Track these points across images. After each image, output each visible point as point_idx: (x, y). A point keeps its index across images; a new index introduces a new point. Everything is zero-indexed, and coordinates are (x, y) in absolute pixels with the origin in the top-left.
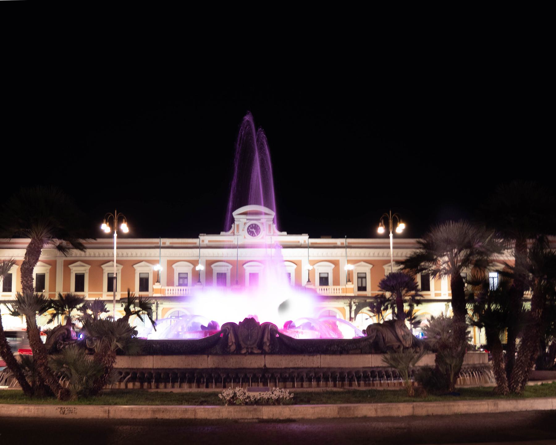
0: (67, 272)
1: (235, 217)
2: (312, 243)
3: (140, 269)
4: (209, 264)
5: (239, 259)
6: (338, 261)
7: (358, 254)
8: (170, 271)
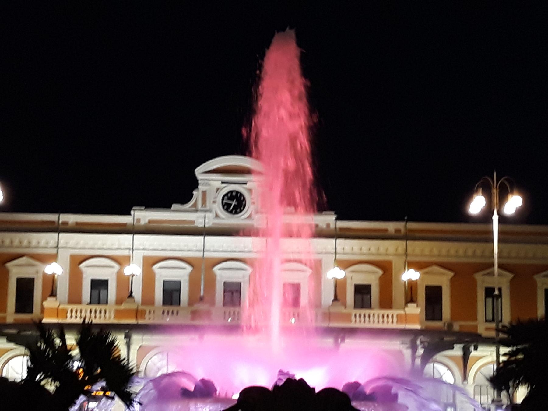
1: (199, 177)
3: (17, 271)
4: (77, 261)
5: (207, 255)
6: (390, 263)
7: (382, 250)
8: (75, 276)
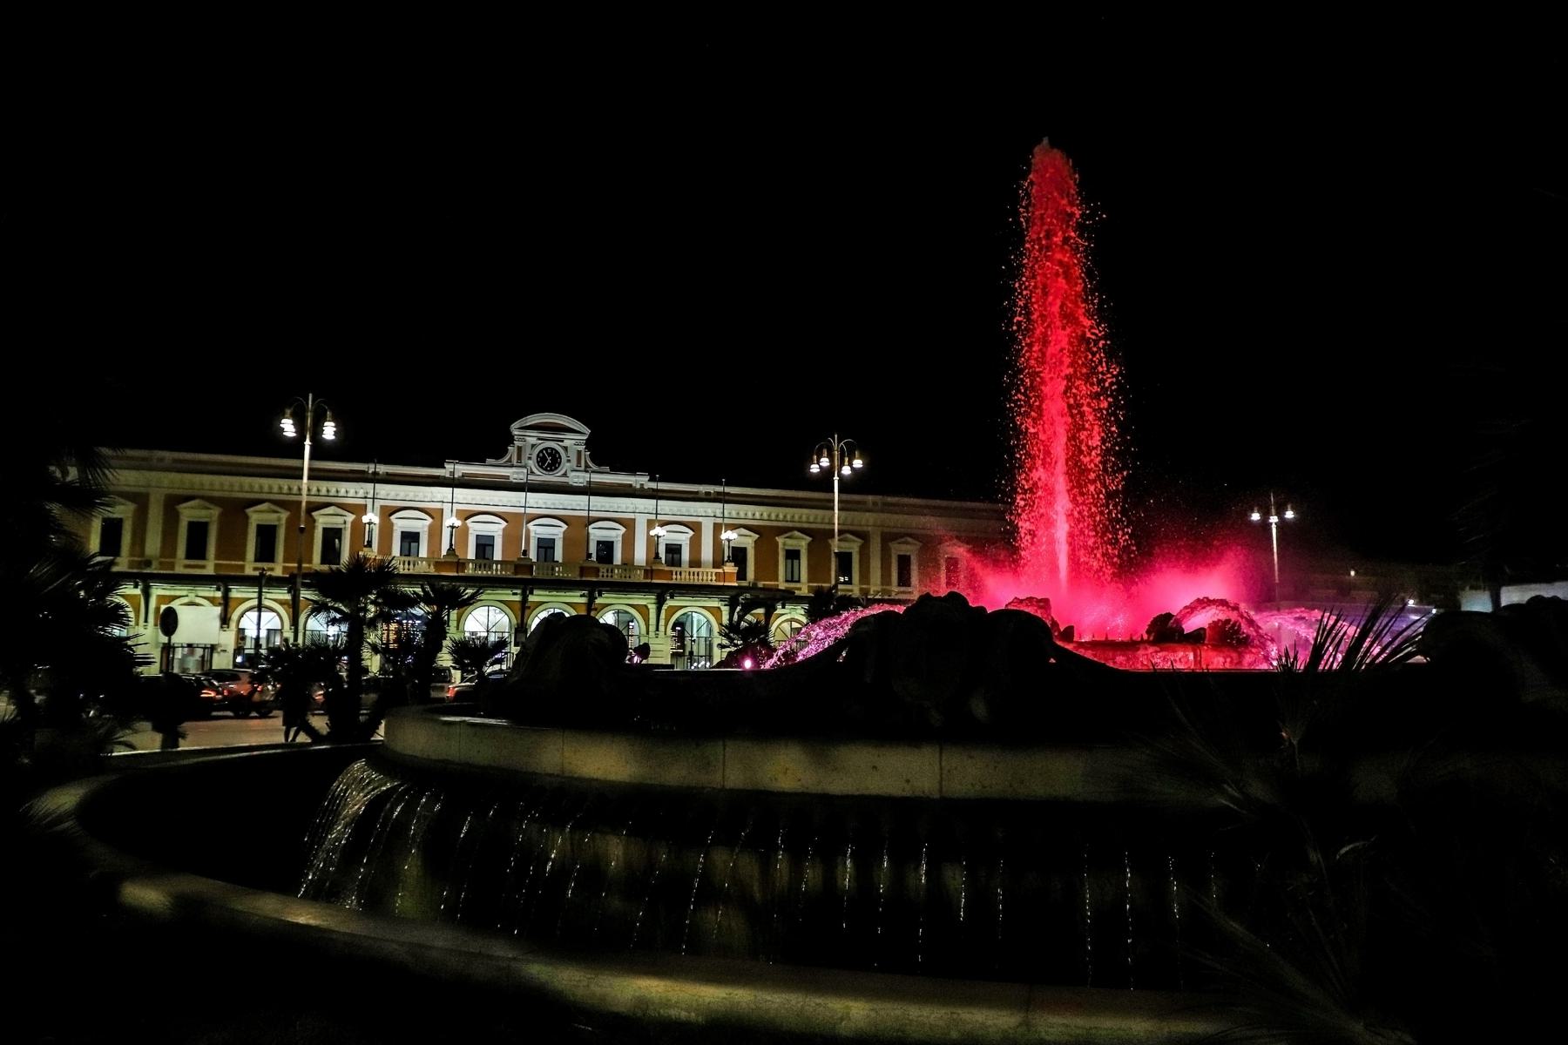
0: (171, 517)
2: (464, 475)
